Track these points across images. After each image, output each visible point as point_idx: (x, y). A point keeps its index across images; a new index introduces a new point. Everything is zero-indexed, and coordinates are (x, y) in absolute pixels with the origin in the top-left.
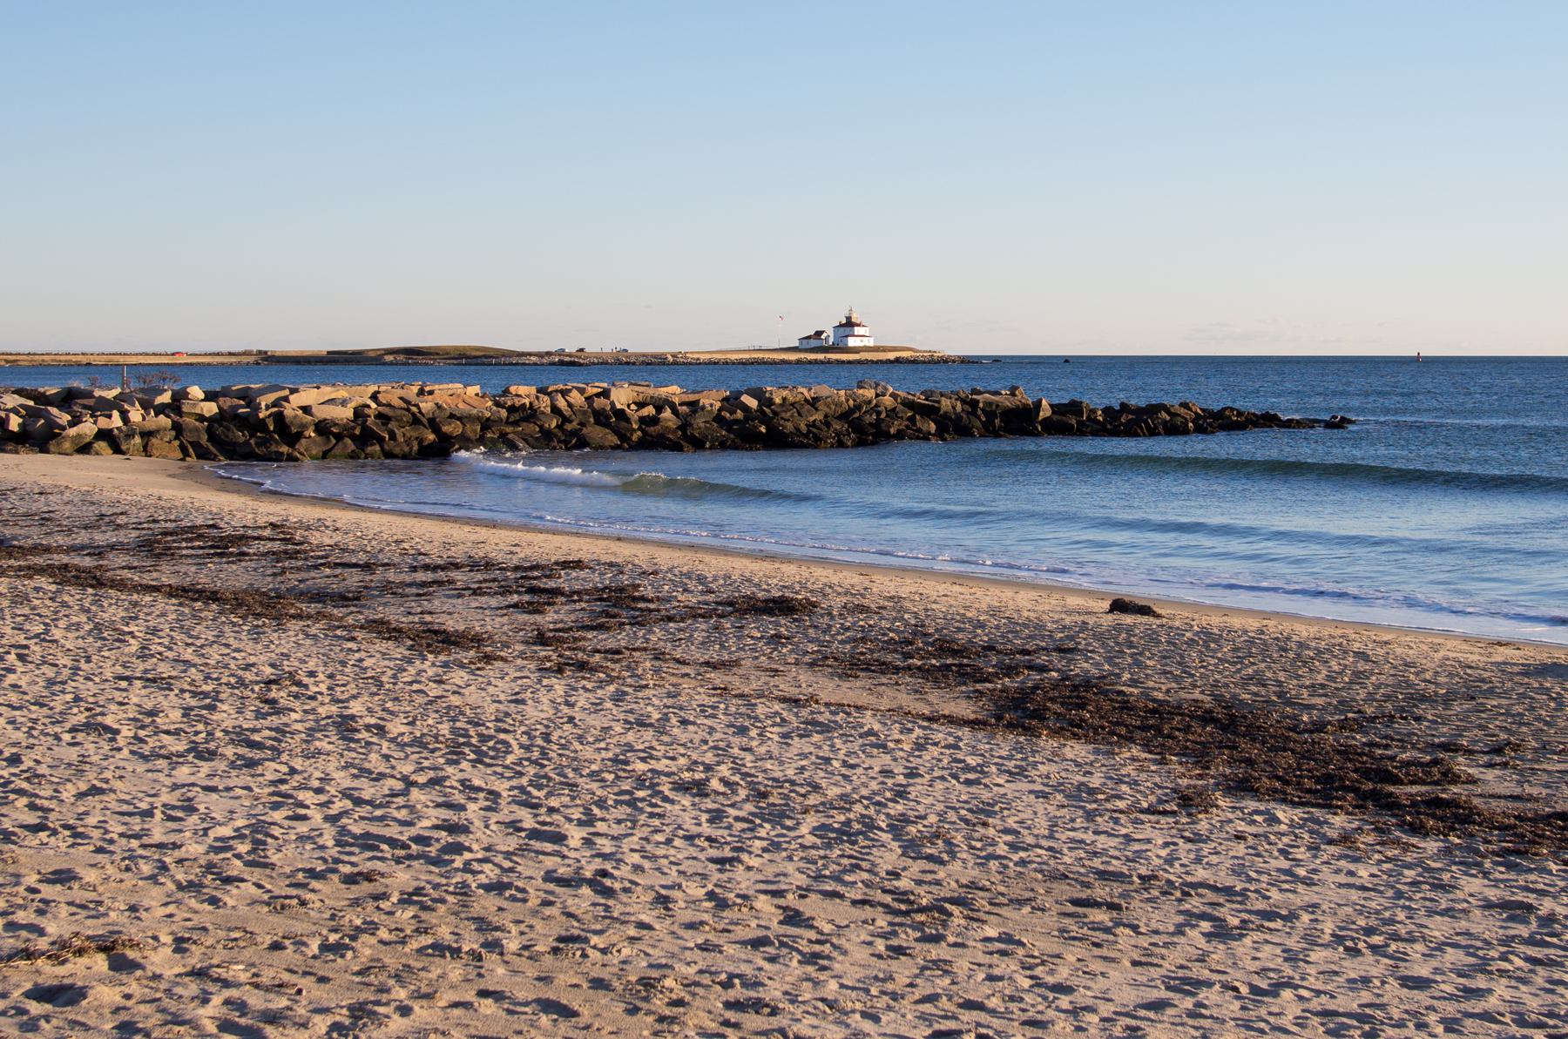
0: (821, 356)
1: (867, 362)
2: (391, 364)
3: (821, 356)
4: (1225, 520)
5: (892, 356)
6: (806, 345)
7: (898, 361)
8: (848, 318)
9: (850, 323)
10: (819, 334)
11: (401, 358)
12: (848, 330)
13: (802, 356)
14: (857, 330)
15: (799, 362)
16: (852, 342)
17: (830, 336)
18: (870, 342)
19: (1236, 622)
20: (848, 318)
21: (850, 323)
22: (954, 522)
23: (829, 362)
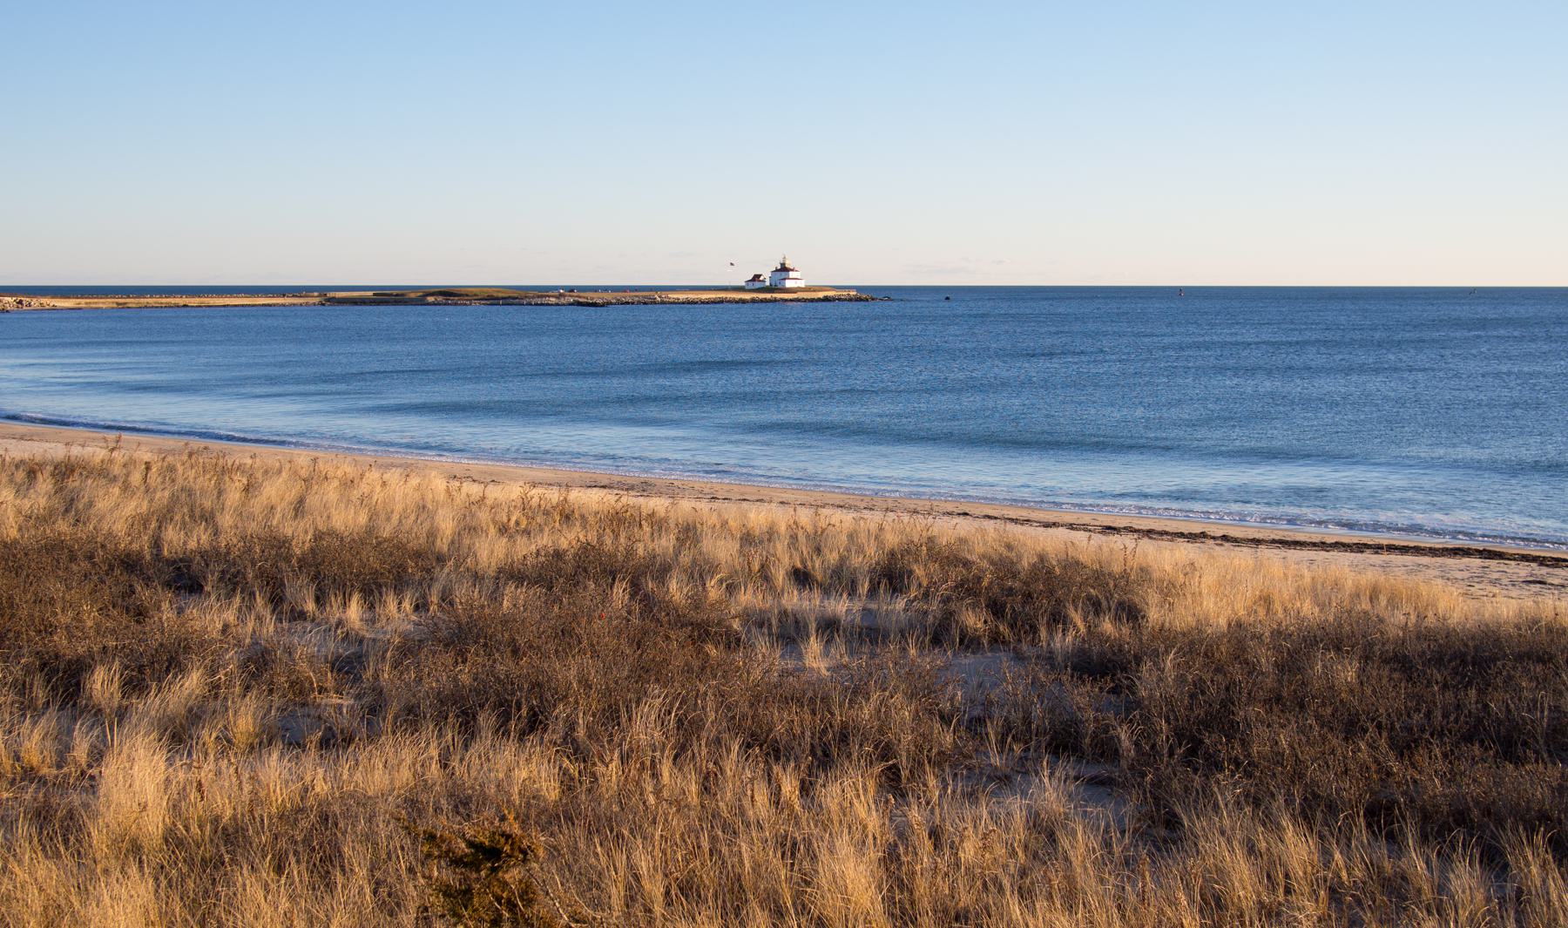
0: (768, 296)
1: (805, 300)
2: (433, 304)
3: (768, 296)
4: (398, 401)
5: (821, 295)
6: (751, 286)
7: (826, 299)
8: (783, 265)
9: (784, 269)
10: (757, 277)
11: (440, 299)
12: (783, 274)
13: (755, 295)
14: (792, 274)
15: (753, 301)
16: (789, 284)
17: (766, 276)
18: (801, 284)
19: (947, 530)
20: (783, 265)
21: (784, 269)
22: (89, 420)
23: (775, 300)
